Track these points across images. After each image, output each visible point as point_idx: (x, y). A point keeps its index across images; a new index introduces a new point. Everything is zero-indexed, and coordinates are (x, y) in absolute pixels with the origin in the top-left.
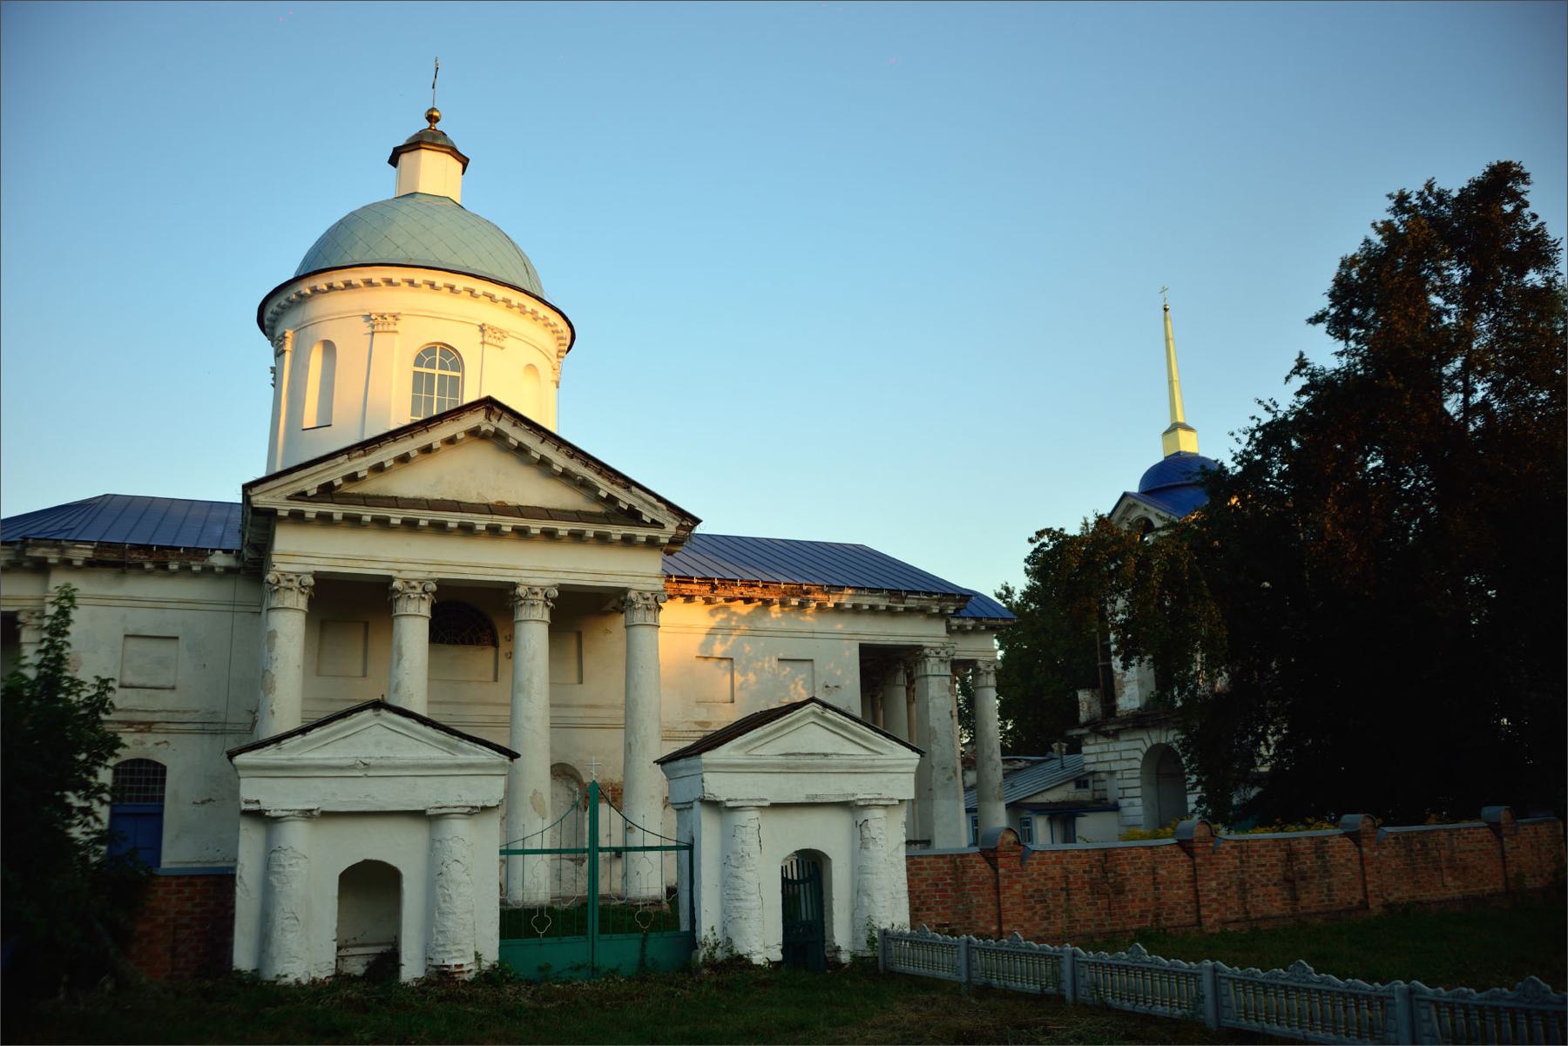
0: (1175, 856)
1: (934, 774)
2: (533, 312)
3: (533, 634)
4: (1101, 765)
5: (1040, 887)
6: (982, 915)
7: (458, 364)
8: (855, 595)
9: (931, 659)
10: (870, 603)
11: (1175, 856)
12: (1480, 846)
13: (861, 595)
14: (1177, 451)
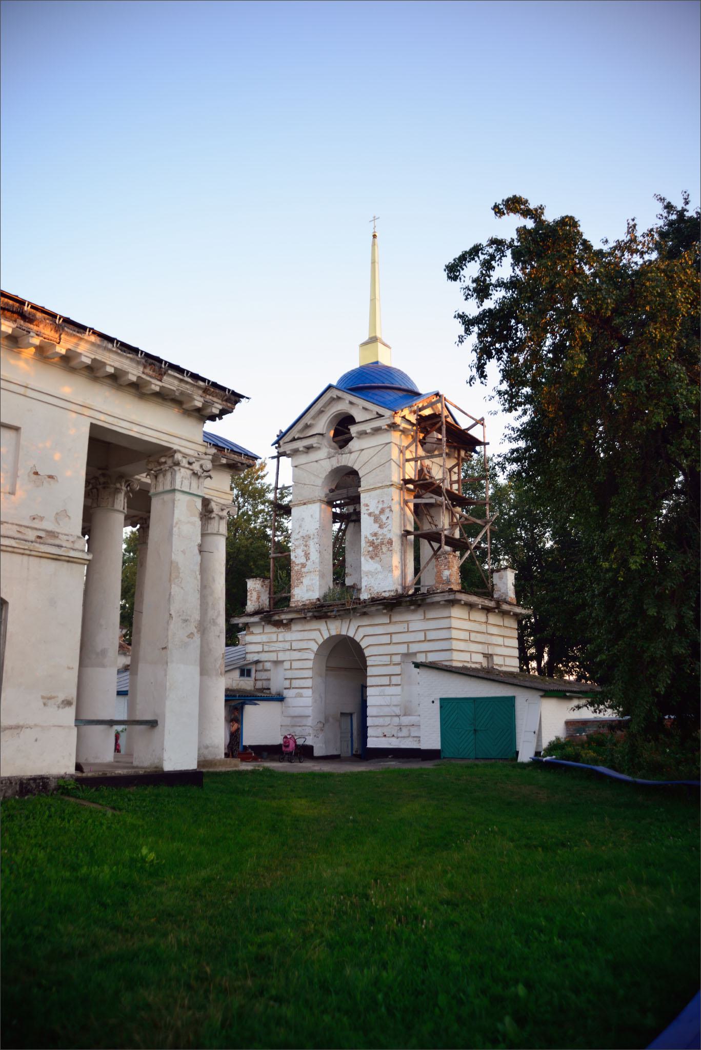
1: (172, 626)
4: (266, 654)
8: (99, 346)
9: (182, 470)
10: (117, 365)
13: (106, 348)
14: (374, 360)
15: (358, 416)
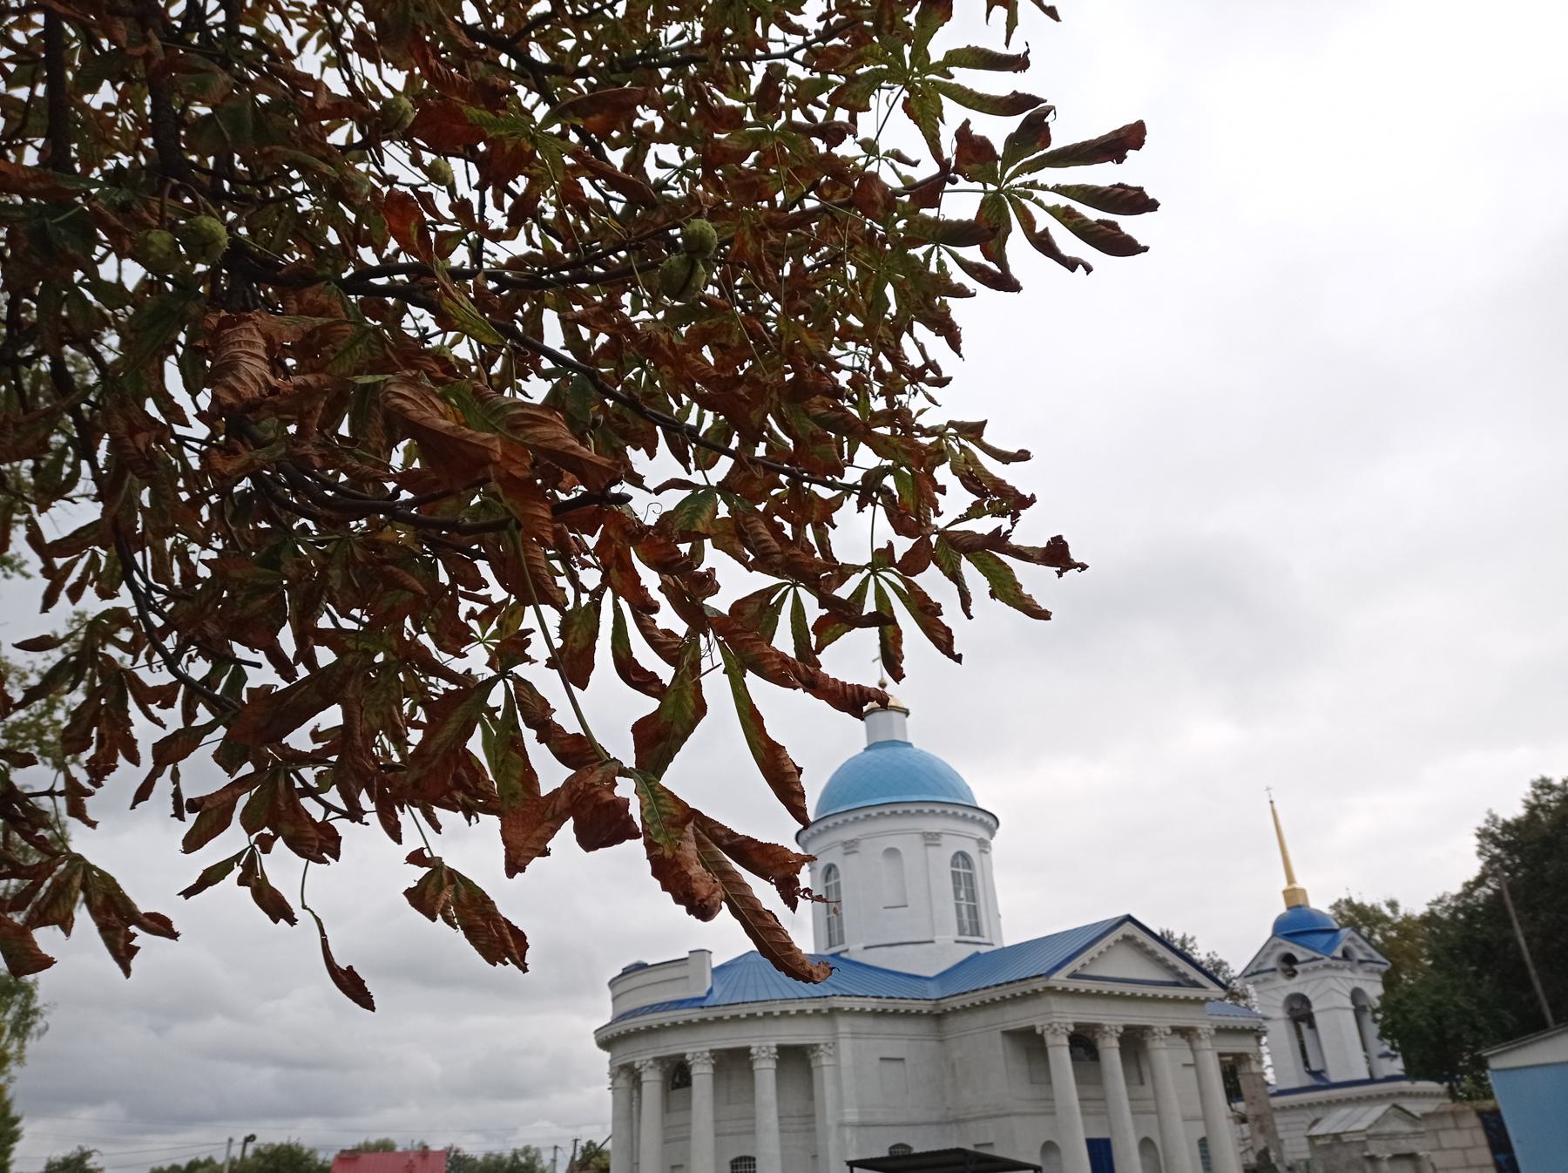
2: (955, 814)
3: (1061, 1055)
15: (1300, 958)
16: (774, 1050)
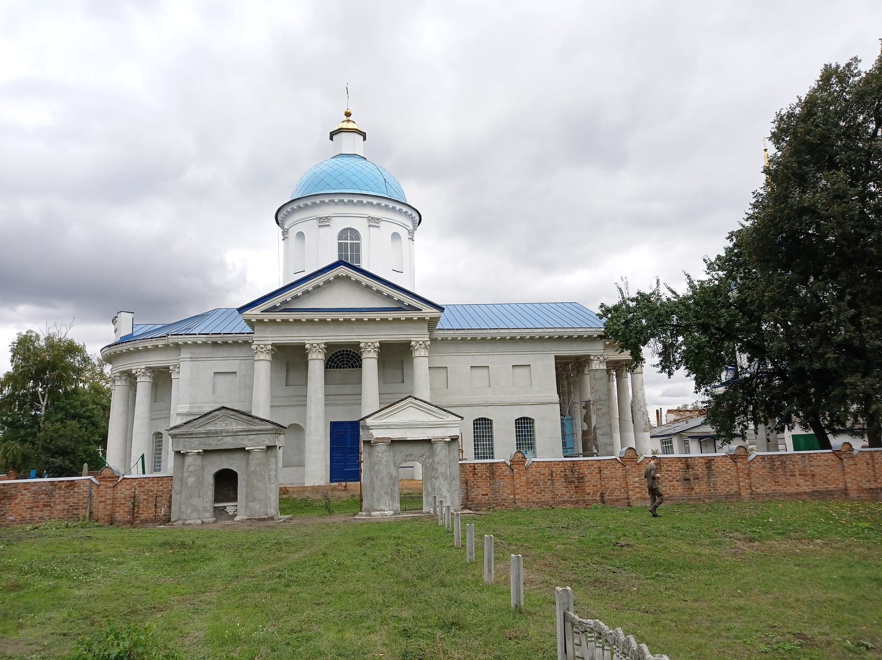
0: (614, 465)
5: (537, 478)
6: (506, 490)
7: (358, 237)
11: (614, 465)
12: (826, 463)
16: (378, 345)
